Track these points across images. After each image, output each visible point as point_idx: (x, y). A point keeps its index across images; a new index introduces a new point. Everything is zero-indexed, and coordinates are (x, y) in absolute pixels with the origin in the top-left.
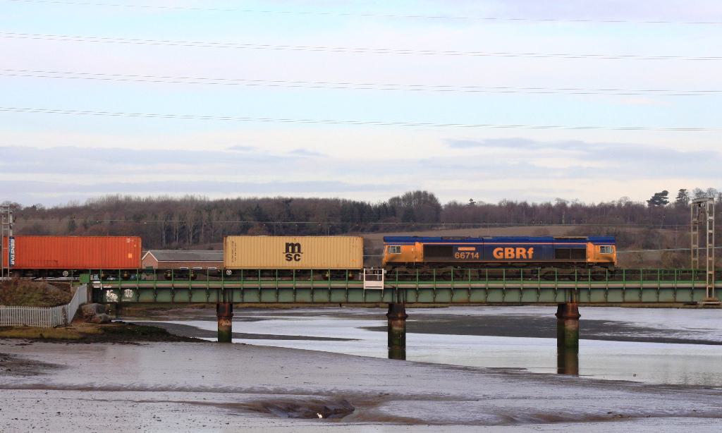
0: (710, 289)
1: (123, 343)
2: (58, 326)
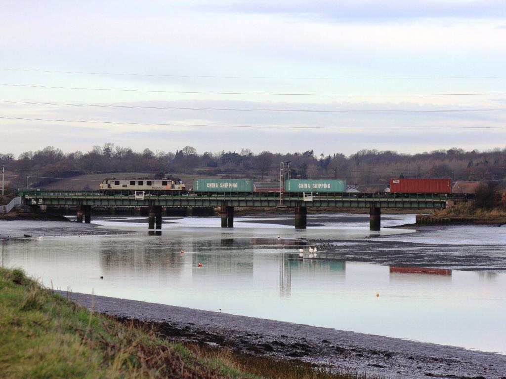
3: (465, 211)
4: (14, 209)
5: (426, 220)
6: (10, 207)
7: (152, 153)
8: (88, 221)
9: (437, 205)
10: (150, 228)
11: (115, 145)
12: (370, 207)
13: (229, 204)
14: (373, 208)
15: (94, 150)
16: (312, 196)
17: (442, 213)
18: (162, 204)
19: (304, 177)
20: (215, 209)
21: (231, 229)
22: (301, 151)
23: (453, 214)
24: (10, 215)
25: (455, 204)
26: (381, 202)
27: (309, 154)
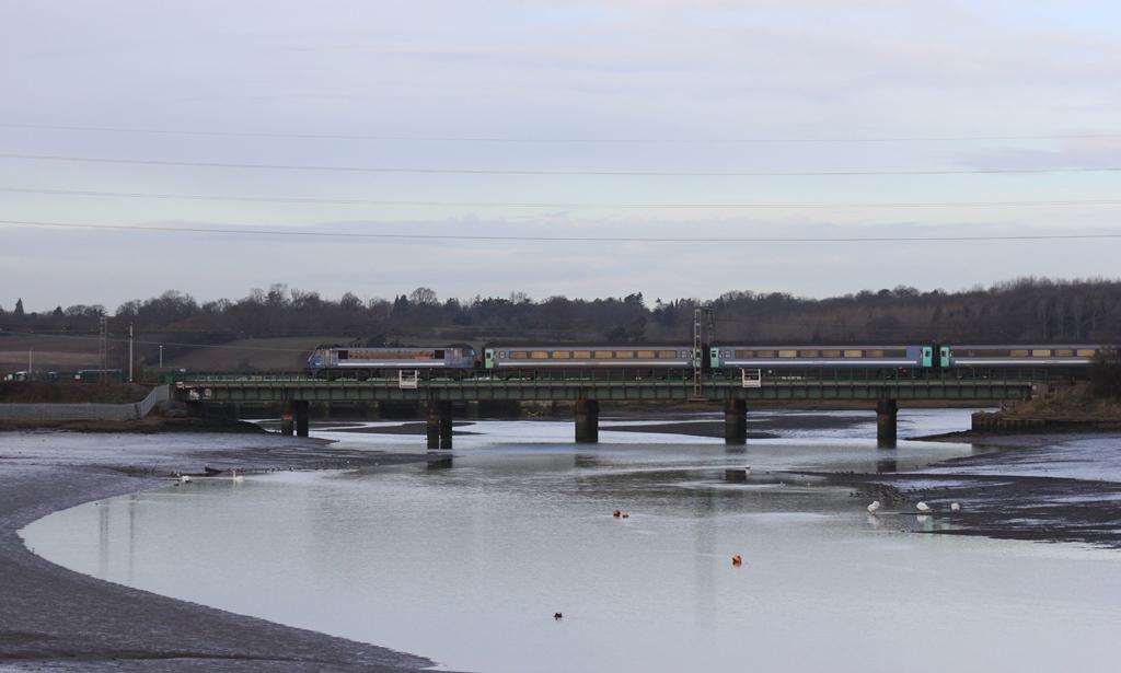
0: (698, 388)
1: (211, 434)
2: (130, 420)
3: (1074, 404)
4: (156, 410)
5: (995, 423)
6: (146, 405)
7: (357, 300)
8: (303, 433)
9: (1014, 393)
10: (430, 446)
11: (290, 287)
12: (877, 399)
13: (591, 396)
14: (884, 401)
15: (164, 296)
16: (416, 379)
17: (1026, 410)
18: (469, 395)
19: (642, 342)
20: (523, 403)
21: (593, 446)
22: (620, 295)
23: (1049, 410)
24: (148, 422)
25: (1051, 390)
26: (899, 388)
27: (634, 301)
